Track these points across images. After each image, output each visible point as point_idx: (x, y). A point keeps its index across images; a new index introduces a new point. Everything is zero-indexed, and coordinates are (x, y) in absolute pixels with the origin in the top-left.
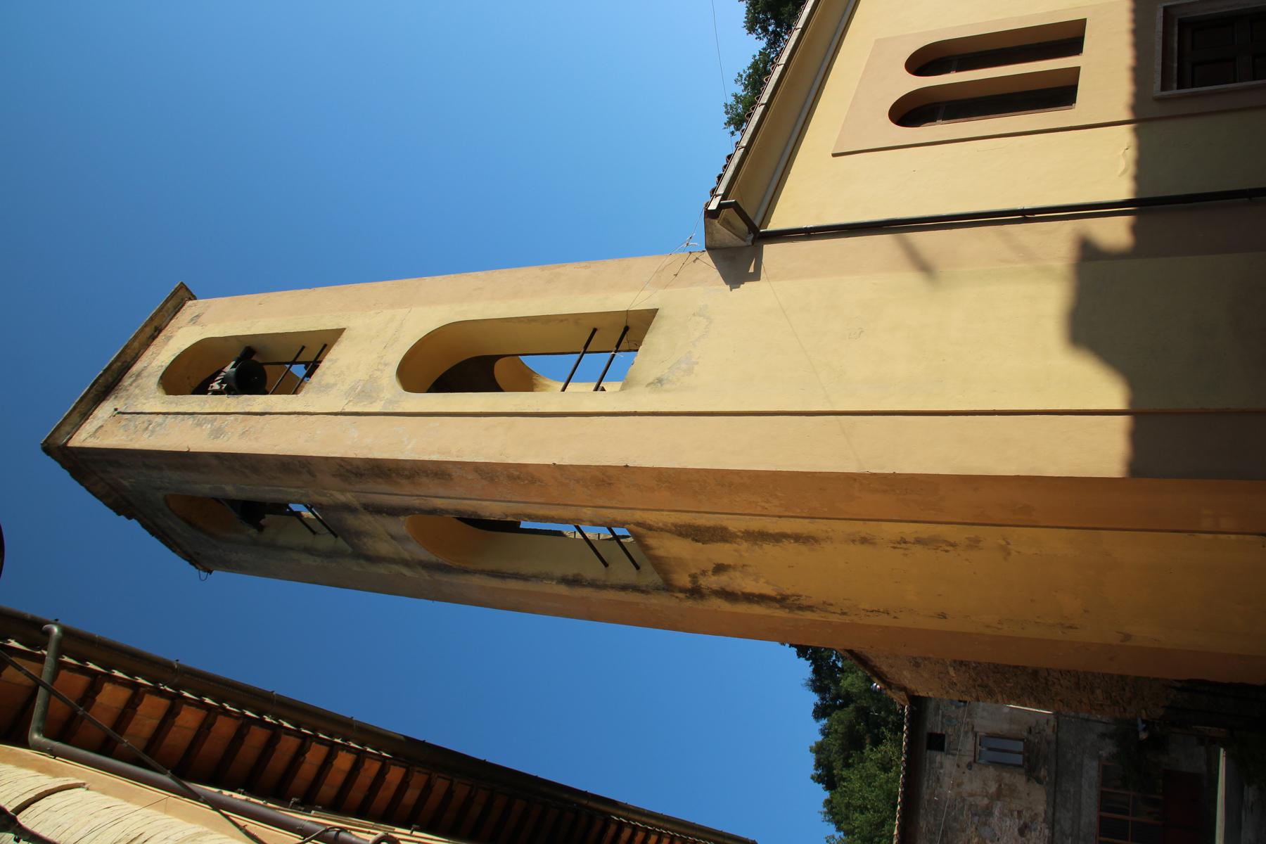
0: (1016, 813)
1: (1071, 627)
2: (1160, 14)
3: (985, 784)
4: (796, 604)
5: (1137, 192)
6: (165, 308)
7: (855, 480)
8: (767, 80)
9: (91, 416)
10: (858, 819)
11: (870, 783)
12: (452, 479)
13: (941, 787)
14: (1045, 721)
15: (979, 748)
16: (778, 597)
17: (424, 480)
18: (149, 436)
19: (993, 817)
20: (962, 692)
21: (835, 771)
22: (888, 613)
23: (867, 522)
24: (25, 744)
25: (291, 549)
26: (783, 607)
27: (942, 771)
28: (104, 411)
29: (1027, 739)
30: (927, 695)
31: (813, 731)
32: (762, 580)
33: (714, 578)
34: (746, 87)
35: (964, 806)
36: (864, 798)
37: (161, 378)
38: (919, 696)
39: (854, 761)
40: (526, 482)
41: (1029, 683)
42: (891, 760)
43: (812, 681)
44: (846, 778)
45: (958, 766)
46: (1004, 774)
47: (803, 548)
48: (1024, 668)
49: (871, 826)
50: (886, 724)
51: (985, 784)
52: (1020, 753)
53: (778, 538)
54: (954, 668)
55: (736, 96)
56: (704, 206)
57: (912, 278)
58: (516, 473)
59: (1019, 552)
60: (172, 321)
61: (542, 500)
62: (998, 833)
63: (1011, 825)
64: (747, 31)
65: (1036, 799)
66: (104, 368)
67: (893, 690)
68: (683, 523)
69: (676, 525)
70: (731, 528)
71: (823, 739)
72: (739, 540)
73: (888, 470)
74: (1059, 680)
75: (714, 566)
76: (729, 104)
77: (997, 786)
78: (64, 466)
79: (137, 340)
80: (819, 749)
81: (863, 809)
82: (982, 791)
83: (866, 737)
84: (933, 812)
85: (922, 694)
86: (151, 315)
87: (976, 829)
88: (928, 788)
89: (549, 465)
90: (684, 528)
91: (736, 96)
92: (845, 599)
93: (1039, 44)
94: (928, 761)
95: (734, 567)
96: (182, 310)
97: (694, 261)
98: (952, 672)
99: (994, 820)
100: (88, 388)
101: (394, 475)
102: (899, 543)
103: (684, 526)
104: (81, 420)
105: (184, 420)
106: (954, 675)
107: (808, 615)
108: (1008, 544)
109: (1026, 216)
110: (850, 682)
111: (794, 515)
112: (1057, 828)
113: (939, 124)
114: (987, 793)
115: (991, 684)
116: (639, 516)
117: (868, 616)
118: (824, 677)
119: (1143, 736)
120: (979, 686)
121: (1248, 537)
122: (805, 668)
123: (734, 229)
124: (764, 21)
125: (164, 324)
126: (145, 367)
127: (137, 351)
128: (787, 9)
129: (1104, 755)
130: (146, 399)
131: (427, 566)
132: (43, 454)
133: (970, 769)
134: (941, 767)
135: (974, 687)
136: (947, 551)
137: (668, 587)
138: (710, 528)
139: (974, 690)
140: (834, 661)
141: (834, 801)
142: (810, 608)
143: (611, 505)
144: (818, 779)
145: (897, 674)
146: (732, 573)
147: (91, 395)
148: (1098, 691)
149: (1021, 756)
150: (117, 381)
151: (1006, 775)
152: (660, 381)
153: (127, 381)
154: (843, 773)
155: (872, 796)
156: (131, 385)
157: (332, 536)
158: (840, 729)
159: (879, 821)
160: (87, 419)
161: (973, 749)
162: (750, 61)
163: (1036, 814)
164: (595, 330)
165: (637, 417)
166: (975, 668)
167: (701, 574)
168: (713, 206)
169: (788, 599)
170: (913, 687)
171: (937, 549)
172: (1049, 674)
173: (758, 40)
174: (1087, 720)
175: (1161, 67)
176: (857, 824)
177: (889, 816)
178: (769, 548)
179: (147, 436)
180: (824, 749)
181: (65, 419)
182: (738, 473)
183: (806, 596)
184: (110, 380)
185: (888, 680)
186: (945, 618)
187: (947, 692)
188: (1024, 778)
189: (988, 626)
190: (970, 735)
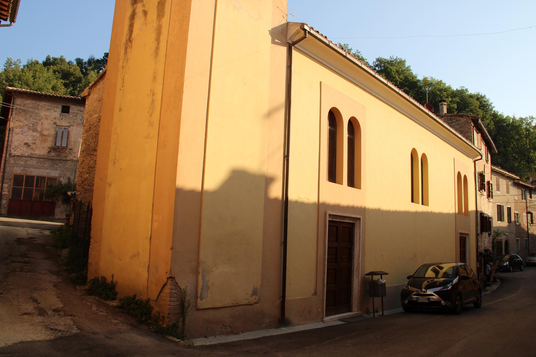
0: (34, 142)
1: (114, 163)
2: (358, 217)
3: (47, 130)
5: (290, 201)
7: (181, 75)
8: (356, 58)
10: (29, 75)
11: (47, 81)
13: (45, 111)
14: (75, 156)
15: (63, 128)
16: (131, 39)
19: (33, 132)
20: (87, 119)
21: (52, 66)
22: (122, 87)
26: (127, 41)
27: (53, 111)
29: (67, 148)
30: (86, 104)
31: (71, 57)
33: (141, 10)
35: (37, 120)
36: (39, 78)
38: (86, 101)
39: (57, 74)
41: (91, 147)
42: (57, 91)
43: (94, 59)
44: (48, 71)
45: (55, 119)
46: (52, 138)
48: (97, 146)
49: (26, 80)
50: (74, 90)
51: (47, 130)
52: (61, 145)
53: (158, 40)
55: (351, 49)
56: (306, 23)
57: (265, 109)
59: (146, 143)
62: (25, 134)
63: (29, 140)
64: (377, 58)
65: (42, 150)
67: (88, 90)
71: (66, 62)
72: (158, 22)
73: (185, 89)
74: (92, 160)
75: (147, 11)
77: (47, 134)
80: (62, 60)
81: (34, 77)
82: (44, 128)
83: (68, 81)
84: (34, 107)
85: (87, 103)
87: (27, 125)
88: (45, 105)
91: (351, 49)
92: (129, 68)
93: (354, 171)
94: (57, 106)
95: (145, 19)
97: (283, 16)
99: (31, 133)
102: (153, 92)
106: (95, 116)
107: (123, 52)
108: (150, 138)
109: (286, 157)
110: (93, 76)
111: (168, 48)
112: (29, 159)
113: (328, 127)
114: (43, 130)
115: (91, 132)
118: (95, 64)
119: (69, 193)
120: (90, 127)
121: (150, 232)
122: (99, 56)
124: (380, 66)
129: (61, 179)
133: (54, 124)
134: (54, 111)
136: (148, 112)
138: (164, 9)
140: (103, 69)
141: (38, 65)
142: (126, 53)
144: (48, 59)
145: (96, 92)
148: (87, 175)
149: (60, 145)
151: (51, 138)
154: (51, 70)
155: (40, 81)
158: (71, 70)
159: (29, 84)
161: (62, 125)
163: (34, 150)
166: (98, 125)
168: (306, 27)
169: (130, 43)
170: (90, 99)
171: (149, 109)
172: (95, 156)
173: (373, 62)
174: (76, 172)
175: (338, 215)
176: (27, 74)
177: (32, 88)
178: (154, 36)
180: (62, 62)
182: (188, 24)
183: (131, 51)
185: (93, 88)
186: (120, 111)
188: (50, 146)
189: (115, 129)
190: (69, 124)
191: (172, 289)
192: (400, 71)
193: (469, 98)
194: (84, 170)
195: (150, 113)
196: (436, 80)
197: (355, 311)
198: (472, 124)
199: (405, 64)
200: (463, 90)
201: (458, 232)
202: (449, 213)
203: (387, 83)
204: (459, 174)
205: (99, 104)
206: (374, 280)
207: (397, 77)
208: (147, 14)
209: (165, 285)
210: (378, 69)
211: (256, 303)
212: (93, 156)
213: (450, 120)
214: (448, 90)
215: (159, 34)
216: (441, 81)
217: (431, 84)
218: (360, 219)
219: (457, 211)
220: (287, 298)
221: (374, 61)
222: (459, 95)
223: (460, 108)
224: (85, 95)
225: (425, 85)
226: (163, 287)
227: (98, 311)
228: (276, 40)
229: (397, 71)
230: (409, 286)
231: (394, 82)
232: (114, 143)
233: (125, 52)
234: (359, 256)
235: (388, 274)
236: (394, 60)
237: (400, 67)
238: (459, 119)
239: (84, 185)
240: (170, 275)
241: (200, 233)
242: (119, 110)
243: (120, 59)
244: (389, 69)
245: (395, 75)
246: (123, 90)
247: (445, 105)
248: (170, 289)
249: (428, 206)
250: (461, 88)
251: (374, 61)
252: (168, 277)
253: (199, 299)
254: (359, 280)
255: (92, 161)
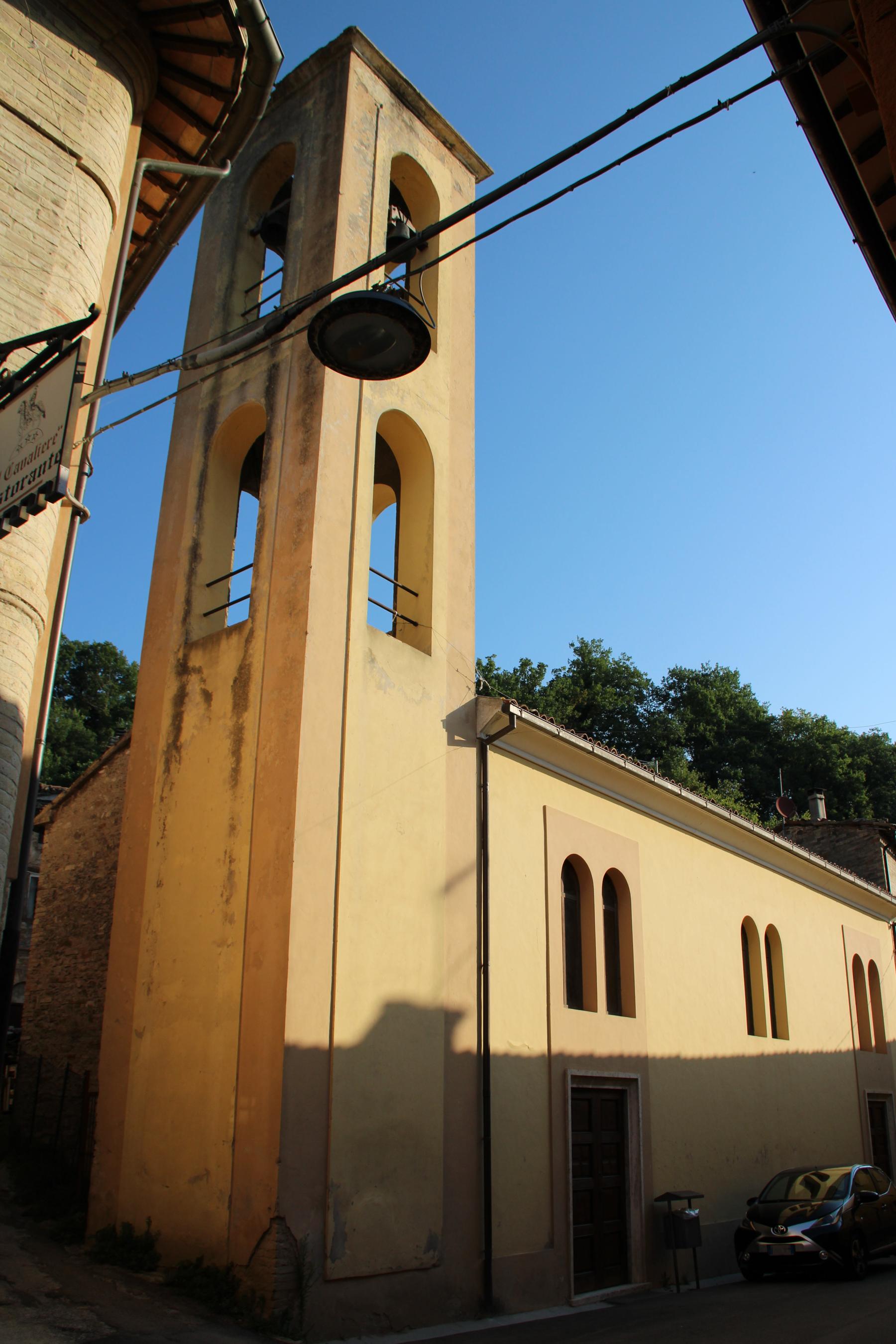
2: (633, 1076)
4: (171, 757)
5: (495, 1056)
6: (471, 156)
7: (288, 828)
9: (377, 77)
12: (300, 464)
17: (301, 436)
18: (355, 148)
23: (250, 833)
24: (140, 156)
25: (233, 268)
26: (169, 746)
28: (381, 93)
32: (196, 732)
34: (616, 663)
37: (407, 155)
40: (295, 536)
41: (58, 937)
47: (227, 773)
53: (236, 753)
54: (74, 870)
55: (609, 652)
57: (440, 877)
58: (304, 529)
59: (220, 954)
60: (458, 162)
61: (277, 546)
66: (421, 94)
67: (51, 811)
68: (252, 673)
69: (250, 665)
70: (246, 715)
72: (235, 719)
73: (296, 856)
74: (61, 964)
75: (210, 692)
76: (602, 643)
78: (332, 43)
79: (444, 128)
86: (466, 142)
89: (310, 561)
90: (247, 672)
91: (609, 652)
92: (176, 802)
93: (620, 979)
96: (468, 172)
98: (69, 868)
100: (405, 77)
101: (307, 406)
102: (230, 857)
103: (249, 672)
104: (374, 67)
105: (367, 185)
106: (66, 869)
107: (160, 767)
108: (228, 946)
109: (483, 967)
111: (258, 772)
115: (56, 903)
116: (260, 634)
117: (160, 820)
123: (492, 724)
124: (680, 687)
125: (457, 154)
126: (418, 135)
127: (434, 125)
128: (688, 712)
130: (389, 141)
131: (213, 410)
132: (346, 27)
135: (54, 887)
136: (222, 895)
137: (189, 645)
138: (247, 695)
139: (50, 886)
142: (167, 770)
143: (270, 611)
146: (203, 706)
147: (397, 79)
148: (49, 999)
150: (408, 104)
152: (373, 660)
153: (407, 115)
156: (403, 121)
157: (243, 312)
160: (375, 73)
162: (642, 670)
164: (416, 595)
165: (345, 641)
167: (202, 678)
178: (227, 745)
179: (355, 145)
181: (377, 52)
184: (410, 99)
187: (48, 861)
191: (280, 1241)
192: (726, 698)
193: (893, 754)
194: (40, 986)
195: (225, 898)
196: (812, 715)
197: (638, 1282)
198: (882, 842)
199: (736, 681)
200: (878, 736)
201: (864, 1091)
202: (838, 1050)
203: (680, 793)
204: (857, 960)
205: (76, 843)
206: (673, 1210)
207: (720, 713)
208: (211, 700)
209: (266, 1233)
210: (674, 695)
211: (434, 1266)
212: (63, 957)
213: (834, 833)
214: (842, 739)
215: (238, 742)
216: (824, 718)
217: (802, 725)
218: (636, 1080)
219: (857, 1045)
220: (496, 1255)
221: (664, 677)
222: (868, 748)
223: (873, 780)
224: (44, 822)
225: (788, 729)
226: (262, 1238)
227: (131, 1294)
228: (456, 736)
229: (720, 700)
230: (751, 1223)
231: (714, 726)
232: (147, 951)
233: (165, 769)
234: (639, 1161)
235: (702, 1196)
236: (711, 674)
237: (727, 689)
238: (853, 831)
239: (42, 1019)
240: (276, 1214)
241: (328, 1127)
242: (156, 885)
243: (156, 780)
244: (700, 696)
245: (714, 708)
246: (163, 844)
247: (821, 799)
248: (276, 1241)
249: (787, 1038)
250: (872, 732)
251: (664, 677)
252: (272, 1217)
253: (329, 1261)
254: (641, 1211)
255: (60, 967)
